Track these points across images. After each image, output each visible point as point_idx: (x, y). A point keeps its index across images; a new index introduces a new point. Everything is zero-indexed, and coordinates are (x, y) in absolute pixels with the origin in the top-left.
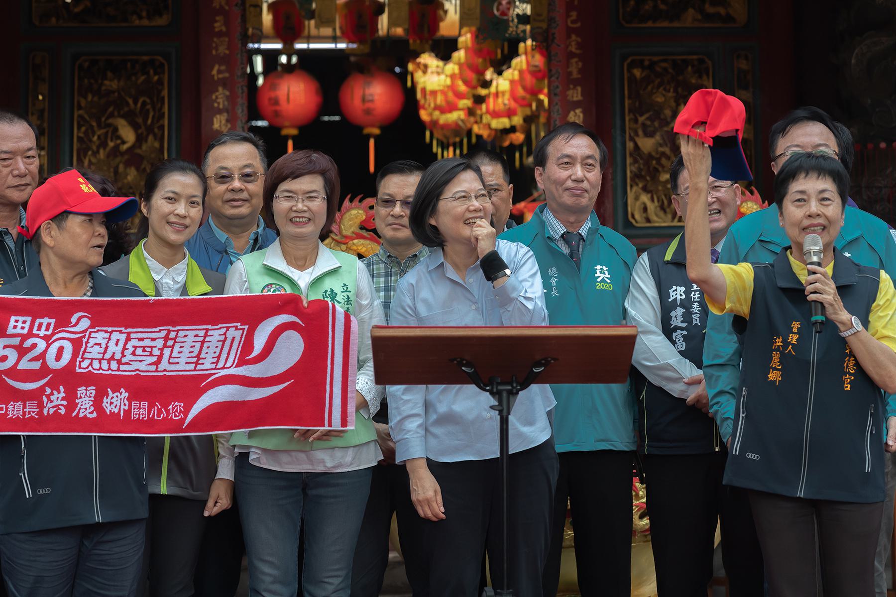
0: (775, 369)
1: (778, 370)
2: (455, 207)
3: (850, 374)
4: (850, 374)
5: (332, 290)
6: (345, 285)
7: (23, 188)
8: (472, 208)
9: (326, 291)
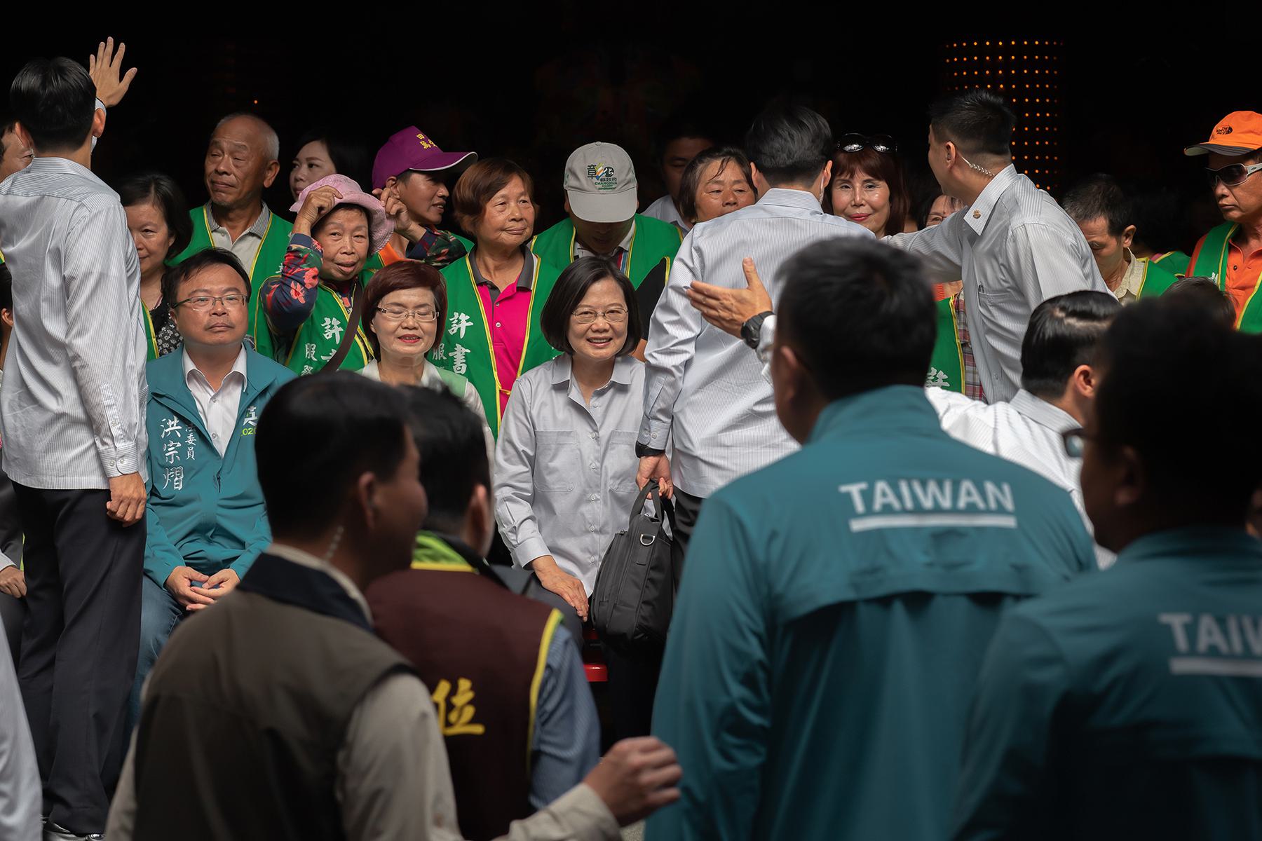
8: (594, 327)
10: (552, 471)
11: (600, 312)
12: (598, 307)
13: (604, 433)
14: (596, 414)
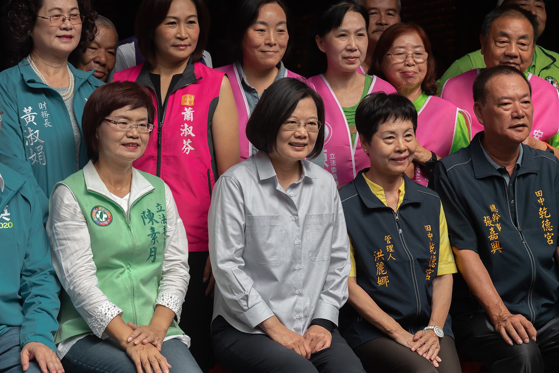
0: (382, 276)
1: (384, 275)
2: (117, 131)
3: (550, 232)
4: (550, 232)
5: (149, 211)
6: (158, 205)
7: (520, 128)
8: (298, 134)
9: (144, 213)
10: (269, 246)
11: (302, 123)
12: (302, 118)
13: (302, 212)
14: (295, 200)
